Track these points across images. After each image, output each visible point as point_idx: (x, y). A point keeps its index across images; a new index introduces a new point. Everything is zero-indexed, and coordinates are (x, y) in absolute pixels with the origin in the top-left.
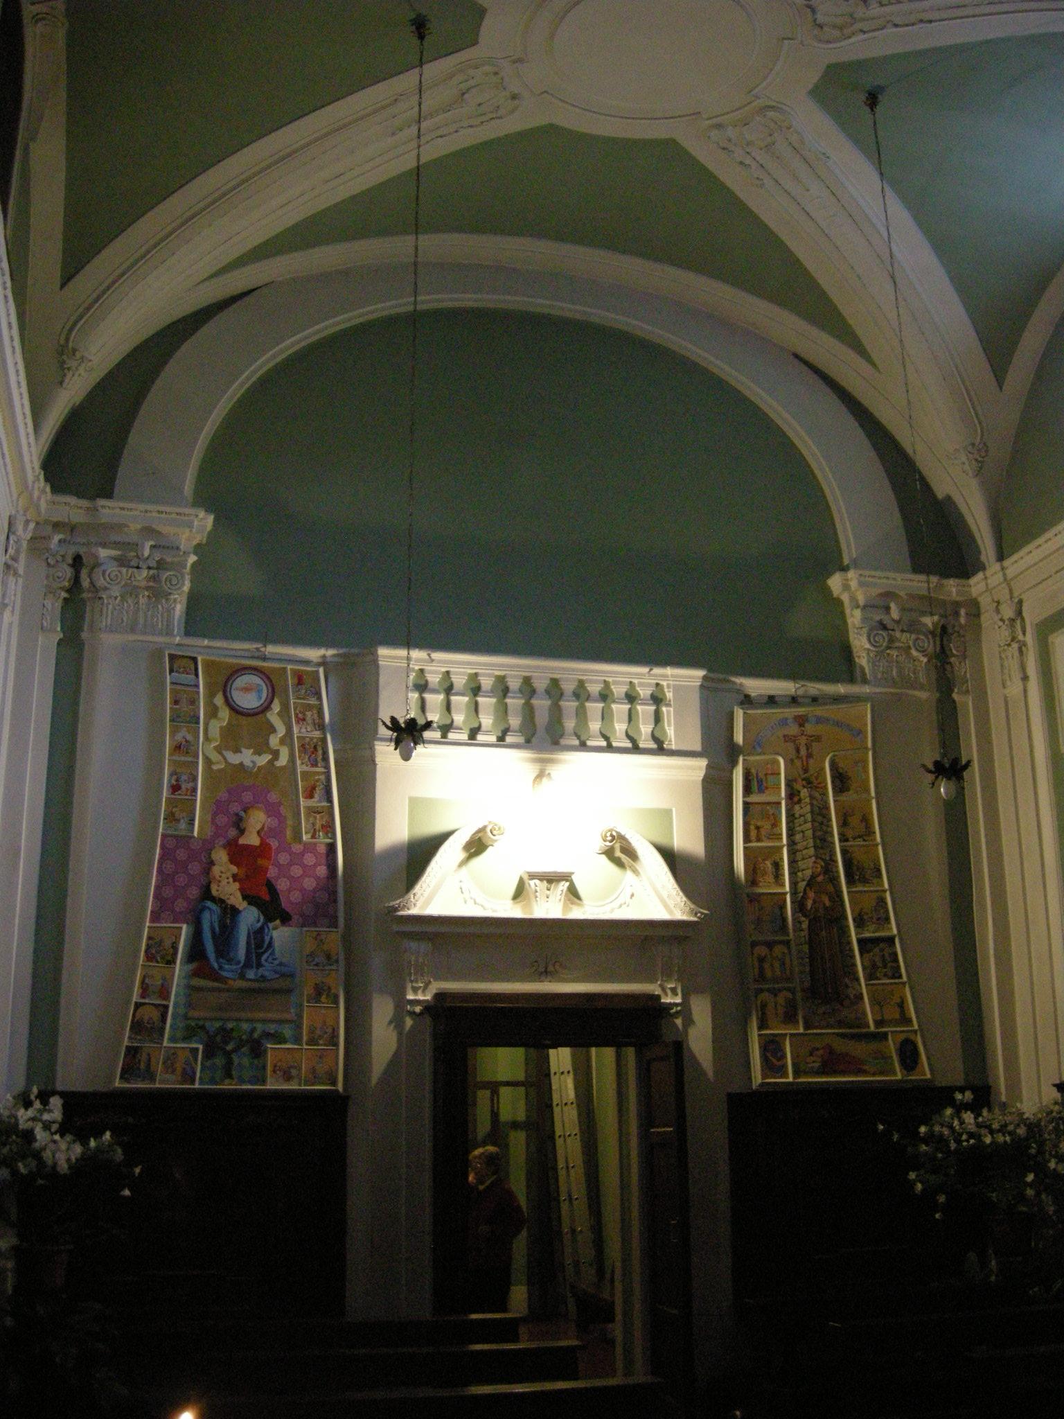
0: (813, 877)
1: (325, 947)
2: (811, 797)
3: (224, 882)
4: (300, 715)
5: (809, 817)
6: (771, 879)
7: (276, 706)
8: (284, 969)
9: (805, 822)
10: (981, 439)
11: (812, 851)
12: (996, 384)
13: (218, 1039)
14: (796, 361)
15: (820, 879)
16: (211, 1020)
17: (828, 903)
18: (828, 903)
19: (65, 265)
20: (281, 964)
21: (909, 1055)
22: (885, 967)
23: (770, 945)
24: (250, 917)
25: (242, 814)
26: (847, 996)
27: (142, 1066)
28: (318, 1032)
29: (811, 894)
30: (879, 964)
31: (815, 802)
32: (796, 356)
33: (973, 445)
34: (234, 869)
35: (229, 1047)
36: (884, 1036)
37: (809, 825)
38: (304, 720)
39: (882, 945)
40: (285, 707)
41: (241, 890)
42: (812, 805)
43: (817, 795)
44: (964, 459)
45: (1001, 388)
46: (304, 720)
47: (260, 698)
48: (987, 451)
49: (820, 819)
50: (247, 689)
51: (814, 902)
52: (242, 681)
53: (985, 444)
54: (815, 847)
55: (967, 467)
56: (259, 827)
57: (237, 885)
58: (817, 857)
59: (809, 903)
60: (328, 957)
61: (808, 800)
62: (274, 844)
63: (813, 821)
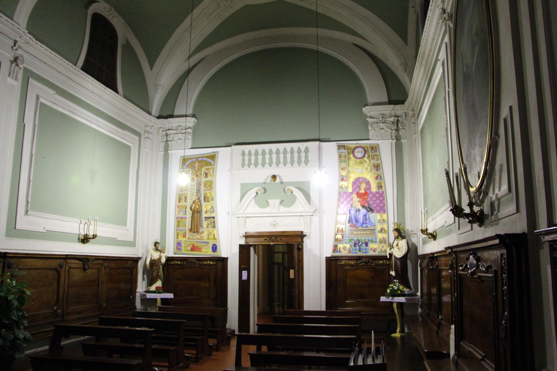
0: (195, 200)
1: (383, 218)
2: (197, 179)
3: (356, 203)
4: (373, 158)
5: (196, 185)
6: (184, 201)
7: (366, 156)
8: (372, 224)
9: (195, 186)
10: (405, 61)
11: (195, 194)
12: (405, 44)
13: (357, 242)
14: (354, 46)
15: (197, 201)
16: (355, 237)
17: (198, 207)
18: (198, 207)
19: (404, 42)
20: (371, 223)
21: (215, 248)
22: (211, 224)
23: (181, 218)
24: (363, 211)
25: (360, 185)
26: (200, 232)
27: (338, 249)
28: (382, 239)
29: (194, 205)
30: (210, 224)
31: (198, 181)
32: (355, 44)
33: (402, 63)
34: (358, 199)
35: (360, 244)
36: (208, 243)
37: (196, 187)
38: (374, 159)
39: (211, 219)
40: (369, 155)
41: (361, 204)
42: (197, 182)
43: (199, 179)
44: (400, 68)
45: (407, 44)
46: (374, 159)
47: (362, 154)
48: (407, 65)
49: (198, 185)
50: (358, 152)
51: (194, 207)
52: (357, 150)
53: (406, 62)
54: (196, 193)
55: (402, 70)
56: (364, 188)
57: (359, 203)
58: (196, 195)
59: (193, 207)
60: (384, 220)
61: (196, 180)
62: (368, 191)
63: (197, 186)
